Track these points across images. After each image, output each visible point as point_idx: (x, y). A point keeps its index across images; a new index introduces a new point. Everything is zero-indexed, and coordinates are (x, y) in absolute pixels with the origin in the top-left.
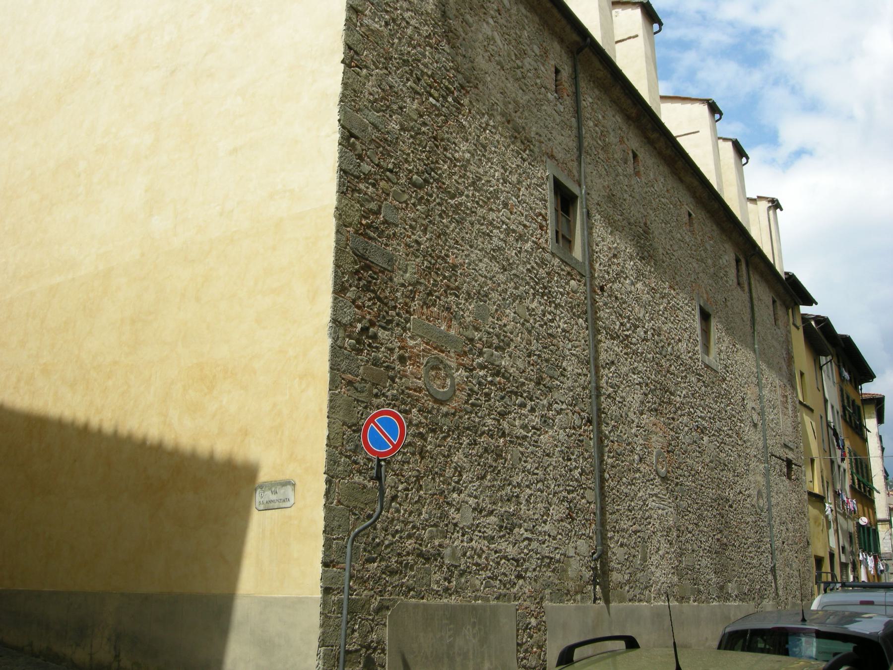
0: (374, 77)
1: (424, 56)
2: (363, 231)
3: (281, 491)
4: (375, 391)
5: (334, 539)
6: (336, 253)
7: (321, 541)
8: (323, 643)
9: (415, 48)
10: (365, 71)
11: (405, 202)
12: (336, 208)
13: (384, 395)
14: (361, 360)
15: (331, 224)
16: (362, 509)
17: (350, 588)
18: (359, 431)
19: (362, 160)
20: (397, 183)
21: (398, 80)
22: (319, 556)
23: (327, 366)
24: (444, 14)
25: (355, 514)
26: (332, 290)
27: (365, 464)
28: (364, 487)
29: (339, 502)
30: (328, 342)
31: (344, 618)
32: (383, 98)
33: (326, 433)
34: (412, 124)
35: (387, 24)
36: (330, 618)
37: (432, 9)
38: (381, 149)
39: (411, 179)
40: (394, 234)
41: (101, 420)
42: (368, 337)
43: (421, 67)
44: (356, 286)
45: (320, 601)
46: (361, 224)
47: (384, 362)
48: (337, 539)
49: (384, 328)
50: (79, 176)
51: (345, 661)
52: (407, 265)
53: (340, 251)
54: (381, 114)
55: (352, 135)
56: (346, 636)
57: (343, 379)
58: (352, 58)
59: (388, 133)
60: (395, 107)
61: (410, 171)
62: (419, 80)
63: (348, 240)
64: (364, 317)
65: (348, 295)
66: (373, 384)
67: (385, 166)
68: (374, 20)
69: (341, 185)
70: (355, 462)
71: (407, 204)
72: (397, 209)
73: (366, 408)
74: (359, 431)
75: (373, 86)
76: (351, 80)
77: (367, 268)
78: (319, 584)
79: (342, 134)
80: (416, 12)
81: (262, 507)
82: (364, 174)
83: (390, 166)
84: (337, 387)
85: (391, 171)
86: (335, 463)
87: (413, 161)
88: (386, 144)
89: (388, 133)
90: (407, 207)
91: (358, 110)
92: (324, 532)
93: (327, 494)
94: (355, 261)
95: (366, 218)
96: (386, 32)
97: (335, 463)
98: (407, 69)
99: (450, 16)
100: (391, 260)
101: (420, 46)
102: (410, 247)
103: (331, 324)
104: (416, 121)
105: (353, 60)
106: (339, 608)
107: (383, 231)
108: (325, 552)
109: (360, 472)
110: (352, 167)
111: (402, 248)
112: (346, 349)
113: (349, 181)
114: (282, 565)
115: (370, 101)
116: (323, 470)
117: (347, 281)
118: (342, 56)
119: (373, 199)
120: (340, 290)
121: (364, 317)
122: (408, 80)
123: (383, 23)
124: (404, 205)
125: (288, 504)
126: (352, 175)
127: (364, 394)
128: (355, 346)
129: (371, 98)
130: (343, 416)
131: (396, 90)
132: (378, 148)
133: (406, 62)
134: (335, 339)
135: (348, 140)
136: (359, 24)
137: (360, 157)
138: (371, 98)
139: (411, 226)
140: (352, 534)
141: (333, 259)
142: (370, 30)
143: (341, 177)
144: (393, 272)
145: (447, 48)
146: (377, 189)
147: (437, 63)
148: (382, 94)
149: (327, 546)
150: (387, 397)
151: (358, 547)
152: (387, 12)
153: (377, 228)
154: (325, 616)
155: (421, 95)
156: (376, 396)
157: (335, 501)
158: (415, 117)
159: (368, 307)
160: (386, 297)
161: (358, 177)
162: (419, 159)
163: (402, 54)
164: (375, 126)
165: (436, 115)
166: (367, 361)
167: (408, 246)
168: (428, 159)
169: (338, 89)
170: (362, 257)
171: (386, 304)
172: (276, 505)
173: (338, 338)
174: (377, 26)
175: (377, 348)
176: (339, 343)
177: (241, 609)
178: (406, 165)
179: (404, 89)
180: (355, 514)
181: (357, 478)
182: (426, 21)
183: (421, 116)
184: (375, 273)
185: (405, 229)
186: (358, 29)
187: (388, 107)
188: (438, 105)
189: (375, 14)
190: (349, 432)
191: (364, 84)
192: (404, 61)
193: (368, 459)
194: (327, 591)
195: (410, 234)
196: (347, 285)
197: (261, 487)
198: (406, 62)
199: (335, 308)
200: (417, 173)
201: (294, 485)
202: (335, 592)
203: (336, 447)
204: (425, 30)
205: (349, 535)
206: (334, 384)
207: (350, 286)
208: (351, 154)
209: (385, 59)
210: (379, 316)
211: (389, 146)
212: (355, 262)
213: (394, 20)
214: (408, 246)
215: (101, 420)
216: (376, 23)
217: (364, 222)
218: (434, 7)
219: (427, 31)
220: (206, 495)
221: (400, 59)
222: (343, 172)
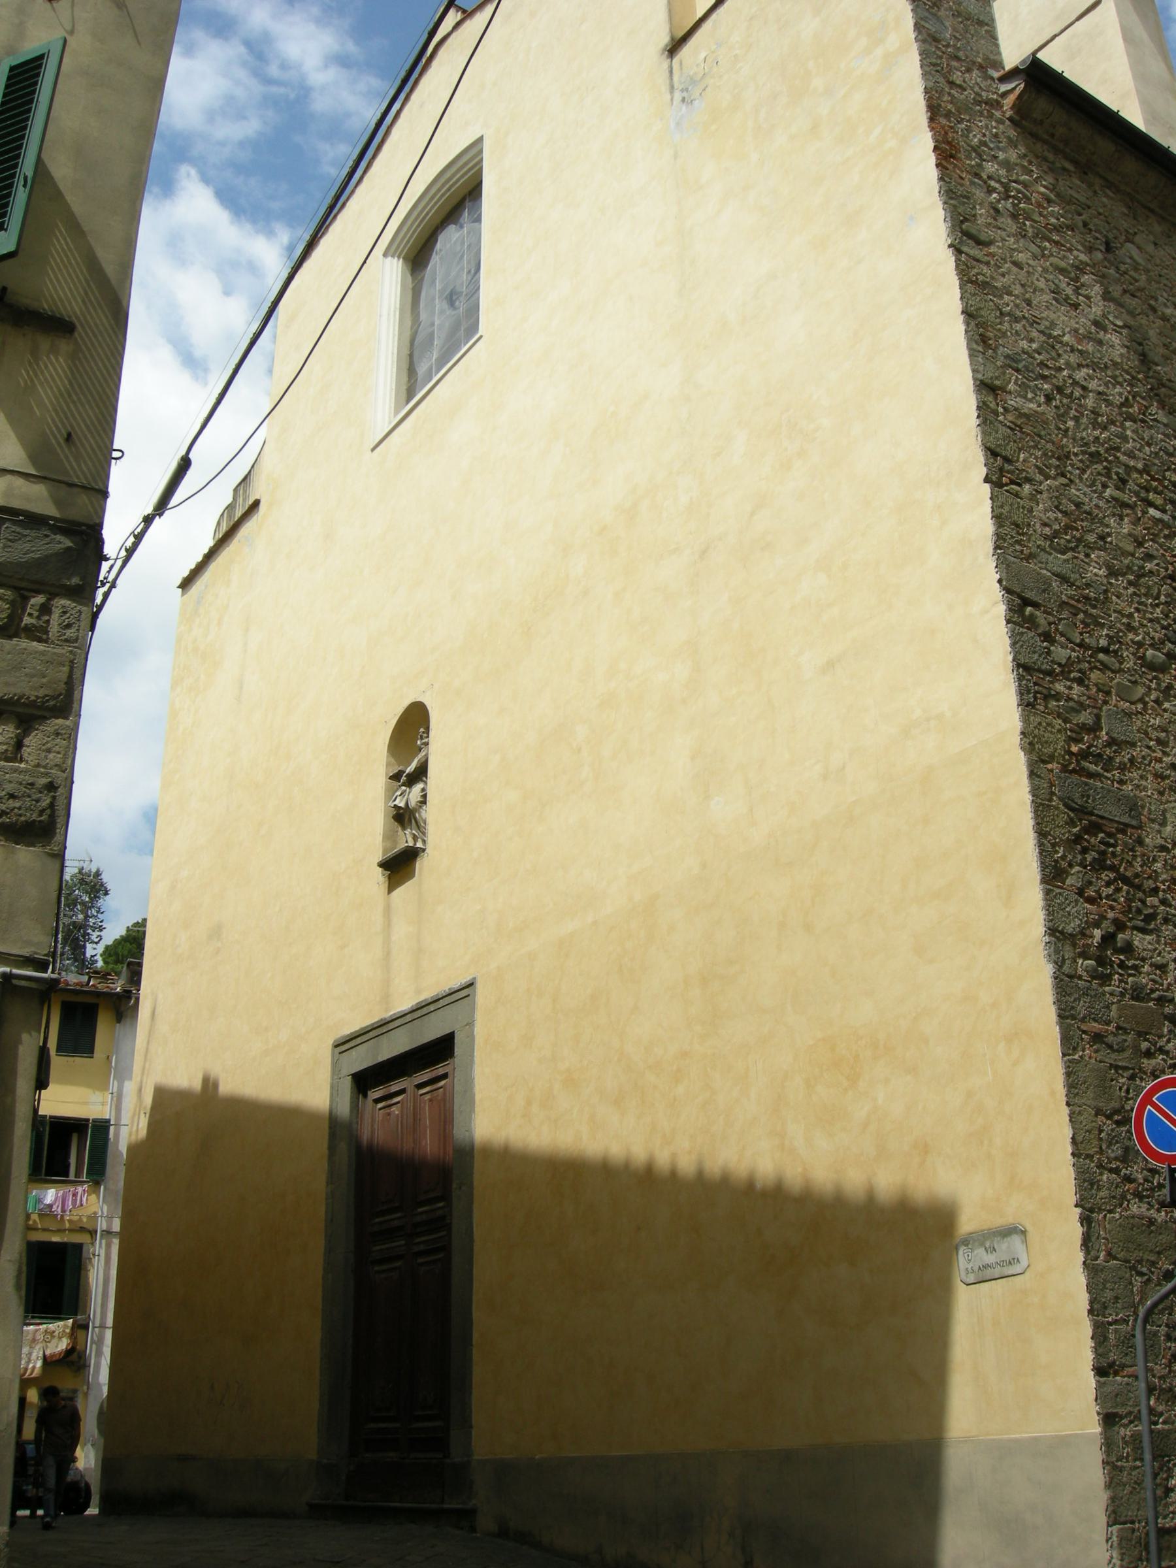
0: (1045, 495)
1: (1125, 439)
2: (1077, 765)
3: (1005, 1247)
4: (1144, 1045)
5: (1110, 1324)
6: (1036, 812)
7: (1087, 1329)
8: (1114, 1517)
9: (1105, 428)
10: (1027, 487)
11: (1141, 700)
12: (1022, 733)
13: (1161, 1050)
14: (1111, 994)
15: (1019, 762)
16: (1153, 1264)
17: (1151, 1411)
18: (1125, 1121)
19: (1052, 641)
20: (1120, 671)
21: (1088, 490)
22: (1087, 1357)
23: (1051, 1014)
24: (1144, 358)
25: (1141, 1274)
26: (1038, 877)
27: (1146, 1180)
28: (1152, 1222)
29: (1110, 1255)
30: (1048, 970)
31: (1148, 1469)
32: (1068, 527)
33: (1069, 1133)
34: (1126, 562)
35: (1049, 398)
36: (1121, 1469)
37: (1121, 355)
38: (1081, 616)
39: (1143, 658)
40: (1132, 760)
41: (674, 1155)
42: (1118, 951)
43: (1123, 458)
44: (1080, 865)
45: (1099, 1440)
46: (1071, 754)
47: (1153, 991)
48: (1115, 1322)
49: (1143, 931)
50: (579, 750)
51: (1160, 1550)
52: (1164, 811)
53: (1041, 808)
54: (1069, 555)
55: (1027, 602)
56: (1156, 1500)
57: (1084, 1032)
58: (1001, 469)
59: (1088, 585)
60: (1091, 538)
61: (1140, 644)
62: (1124, 482)
63: (1052, 785)
64: (1103, 917)
65: (1068, 882)
66: (1139, 1034)
67: (1093, 644)
68: (1025, 397)
69: (1022, 692)
70: (1128, 1179)
71: (1145, 704)
72: (1129, 715)
73: (1132, 1078)
74: (1127, 1121)
75: (1046, 510)
76: (1007, 508)
77: (1093, 828)
78: (1094, 1408)
79: (1009, 603)
80: (1094, 366)
81: (971, 1278)
82: (1060, 665)
83: (1103, 642)
84: (1075, 1049)
85: (1105, 651)
86: (1092, 1184)
87: (1142, 625)
88: (1087, 605)
89: (1088, 585)
90: (1145, 708)
91: (1030, 557)
92: (1090, 1312)
93: (1087, 1242)
94: (1071, 819)
95: (1077, 741)
96: (1049, 412)
97: (1092, 1184)
98: (1099, 467)
99: (1156, 360)
100: (1134, 807)
101: (1113, 422)
102: (1163, 778)
103: (1047, 939)
104: (1133, 555)
105: (1002, 474)
106: (1135, 1449)
107: (1111, 759)
108: (1096, 1350)
109: (1139, 1196)
110: (1036, 656)
111: (1150, 783)
112: (1080, 978)
113: (1035, 681)
114: (1020, 1373)
115: (1046, 537)
116: (1073, 1199)
117: (1063, 858)
118: (984, 471)
119: (1082, 705)
120: (1052, 875)
121: (1103, 917)
122: (1105, 486)
123: (1042, 399)
124: (1140, 706)
125: (1017, 1269)
126: (1040, 671)
127: (1126, 1054)
128: (1096, 970)
129: (1047, 531)
130: (1095, 1099)
131: (1086, 508)
132: (1076, 615)
133: (1095, 457)
134: (1059, 964)
135: (1021, 611)
136: (1001, 410)
137: (1047, 637)
138: (1047, 531)
139: (1159, 741)
140: (1142, 1311)
141: (1031, 823)
142: (1022, 415)
143: (1020, 678)
144: (1140, 827)
145: (1162, 416)
146: (1087, 687)
147: (1149, 445)
148: (1064, 521)
149: (1100, 1337)
150: (1167, 1053)
151: (1155, 1334)
152: (1044, 377)
153: (1100, 755)
154: (1112, 1466)
155: (1132, 507)
156: (1149, 1054)
157: (1102, 1255)
158: (1130, 548)
159: (1108, 897)
160: (1137, 875)
161: (1050, 673)
162: (1151, 621)
163: (1086, 444)
164: (1064, 579)
165: (1166, 537)
166: (1122, 995)
167: (1159, 776)
168: (1167, 616)
169: (987, 527)
170: (1082, 811)
171: (1139, 887)
172: (997, 1272)
173: (1064, 960)
174: (1033, 406)
175: (1135, 967)
176: (1066, 969)
177: (958, 1466)
178: (1131, 636)
179: (1101, 504)
180: (1141, 1274)
181: (1136, 1208)
182: (1114, 377)
183: (1140, 544)
184: (1110, 835)
185: (1149, 747)
186: (1001, 418)
187: (1079, 540)
188: (1166, 518)
189: (1024, 386)
190: (1109, 1126)
191: (1031, 511)
192: (1091, 455)
193: (1150, 1170)
194: (1109, 1420)
195: (1159, 755)
196: (1064, 864)
197: (966, 1242)
198: (1095, 457)
199: (1051, 909)
200: (1152, 646)
201: (1024, 1233)
202: (1125, 1421)
203: (1089, 1157)
204: (1117, 394)
205: (1136, 1314)
206: (1069, 1044)
207: (1071, 866)
208: (1031, 634)
209: (1058, 459)
210: (1130, 911)
211: (1094, 607)
212: (1072, 823)
213: (1060, 390)
214: (1159, 776)
215: (674, 1155)
216: (1030, 401)
217: (1074, 749)
218: (1124, 351)
219: (1120, 394)
220: (876, 1263)
221: (1084, 453)
222: (1023, 668)
